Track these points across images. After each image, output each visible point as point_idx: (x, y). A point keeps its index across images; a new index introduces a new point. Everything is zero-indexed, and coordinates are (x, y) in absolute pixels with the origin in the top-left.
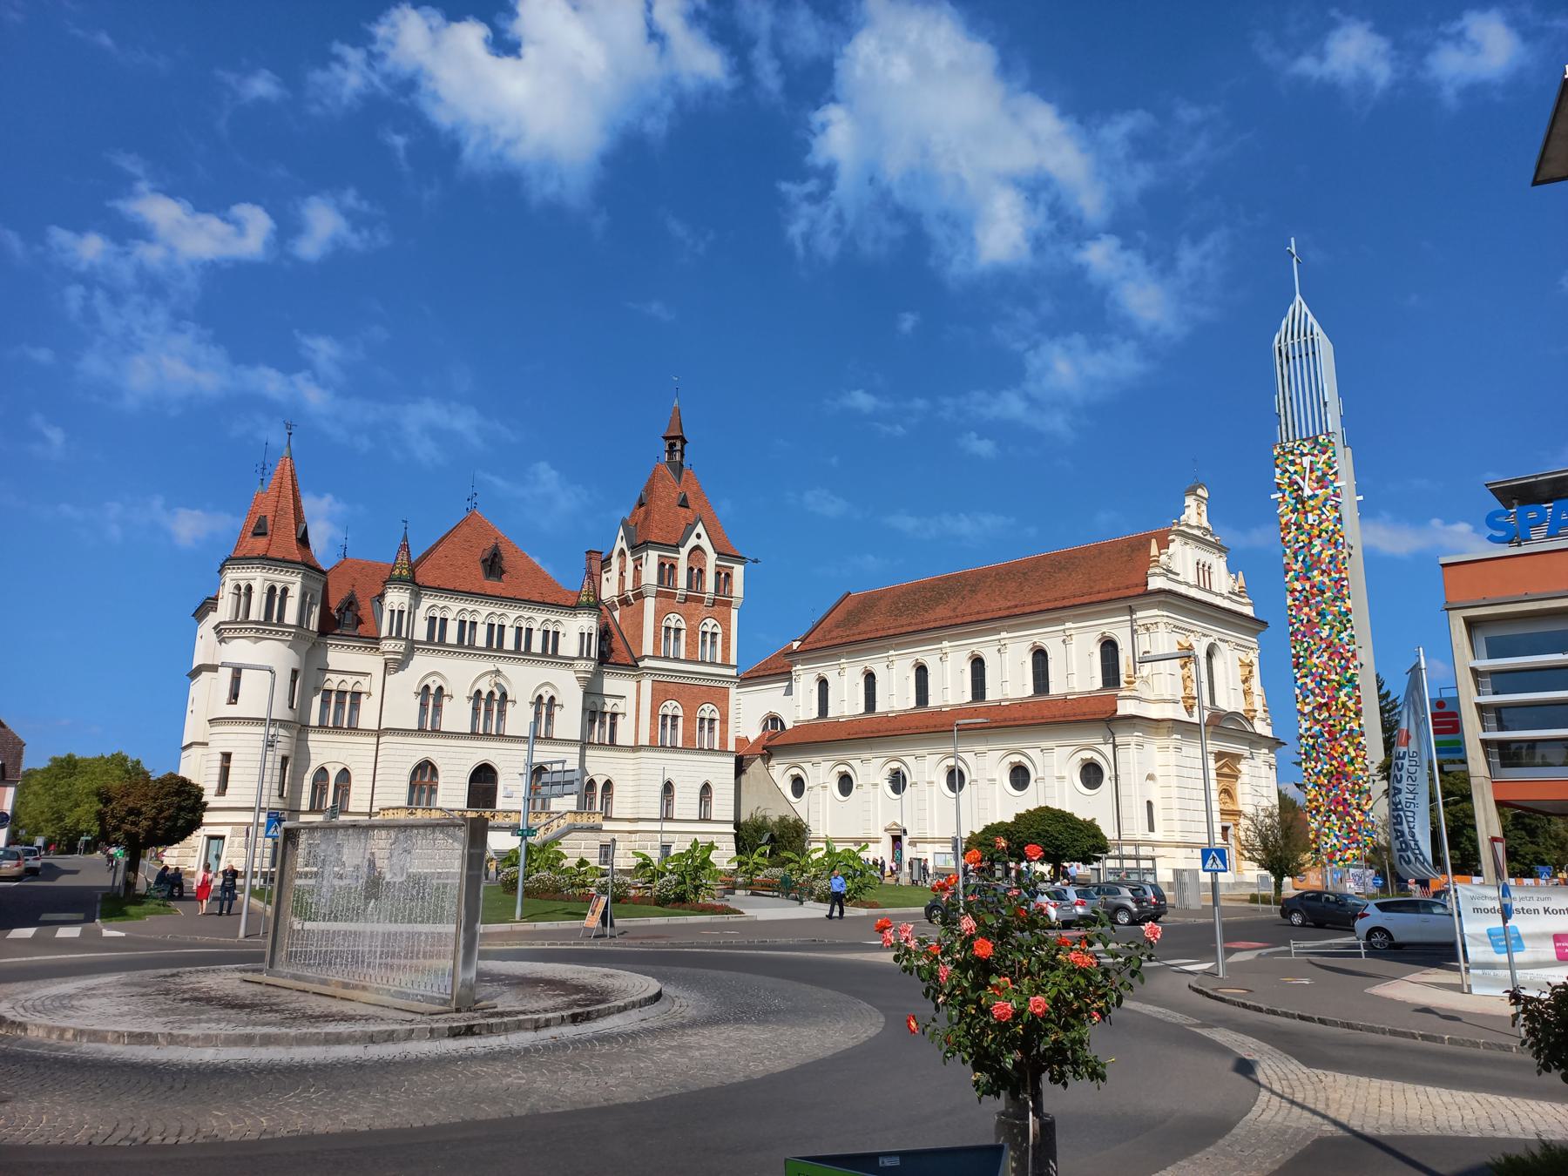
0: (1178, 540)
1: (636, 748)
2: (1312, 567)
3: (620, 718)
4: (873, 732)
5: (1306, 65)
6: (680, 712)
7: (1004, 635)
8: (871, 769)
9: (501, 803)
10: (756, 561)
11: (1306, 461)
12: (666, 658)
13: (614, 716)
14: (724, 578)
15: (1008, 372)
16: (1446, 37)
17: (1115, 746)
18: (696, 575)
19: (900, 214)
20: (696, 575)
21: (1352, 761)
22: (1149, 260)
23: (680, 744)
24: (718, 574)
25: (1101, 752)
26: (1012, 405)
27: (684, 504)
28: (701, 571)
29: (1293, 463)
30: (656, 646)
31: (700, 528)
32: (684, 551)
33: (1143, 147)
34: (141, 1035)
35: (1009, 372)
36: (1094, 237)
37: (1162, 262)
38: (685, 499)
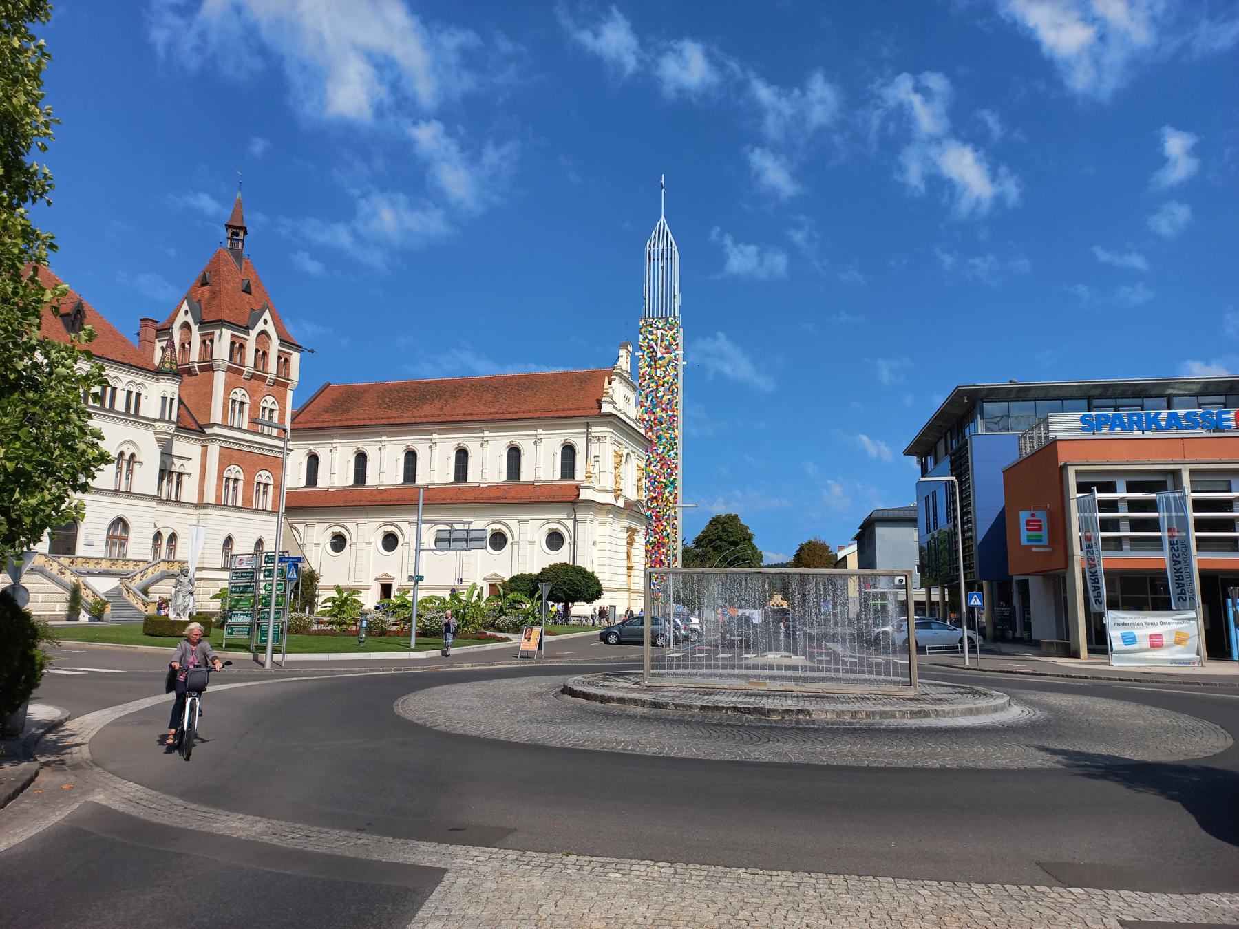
0: (618, 379)
1: (201, 505)
2: (657, 406)
3: (185, 478)
4: (361, 500)
5: (586, 37)
6: (241, 477)
7: (486, 433)
8: (365, 532)
9: (81, 550)
10: (312, 351)
11: (660, 332)
12: (232, 427)
13: (180, 475)
14: (284, 362)
15: (342, 210)
16: (674, 51)
17: (575, 521)
18: (262, 355)
19: (262, 50)
20: (262, 355)
21: (668, 535)
22: (463, 148)
23: (239, 504)
24: (279, 358)
25: (563, 524)
26: (340, 236)
27: (247, 290)
28: (265, 353)
29: (651, 333)
30: (225, 416)
31: (267, 315)
32: (253, 334)
33: (470, 60)
34: (919, 712)
35: (344, 211)
36: (427, 118)
37: (471, 152)
38: (248, 286)
